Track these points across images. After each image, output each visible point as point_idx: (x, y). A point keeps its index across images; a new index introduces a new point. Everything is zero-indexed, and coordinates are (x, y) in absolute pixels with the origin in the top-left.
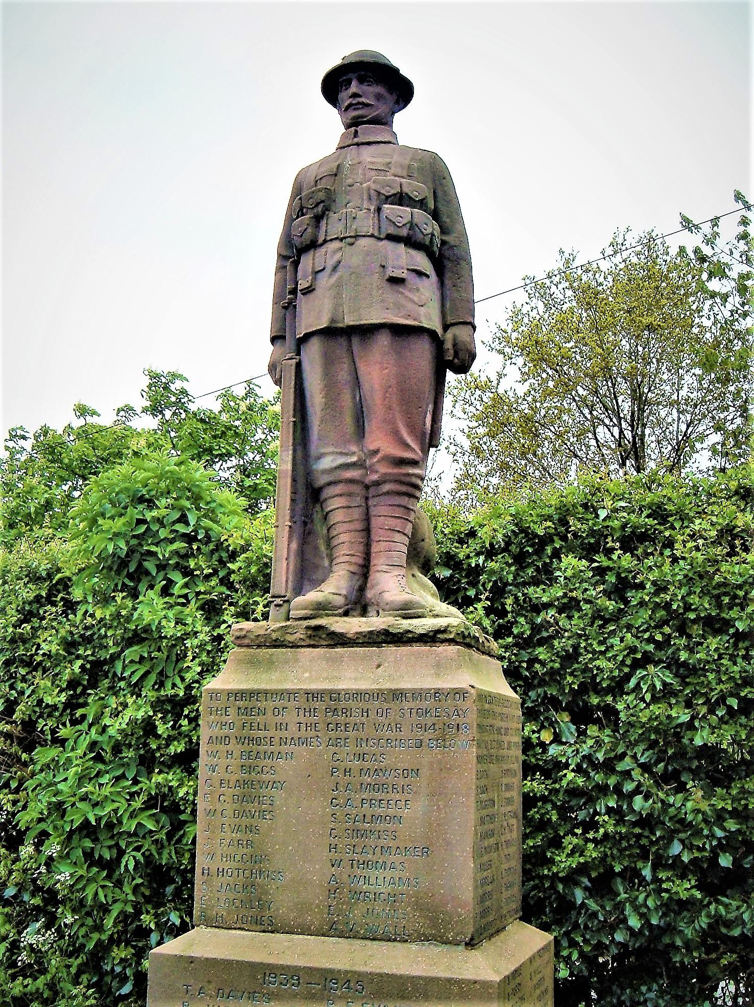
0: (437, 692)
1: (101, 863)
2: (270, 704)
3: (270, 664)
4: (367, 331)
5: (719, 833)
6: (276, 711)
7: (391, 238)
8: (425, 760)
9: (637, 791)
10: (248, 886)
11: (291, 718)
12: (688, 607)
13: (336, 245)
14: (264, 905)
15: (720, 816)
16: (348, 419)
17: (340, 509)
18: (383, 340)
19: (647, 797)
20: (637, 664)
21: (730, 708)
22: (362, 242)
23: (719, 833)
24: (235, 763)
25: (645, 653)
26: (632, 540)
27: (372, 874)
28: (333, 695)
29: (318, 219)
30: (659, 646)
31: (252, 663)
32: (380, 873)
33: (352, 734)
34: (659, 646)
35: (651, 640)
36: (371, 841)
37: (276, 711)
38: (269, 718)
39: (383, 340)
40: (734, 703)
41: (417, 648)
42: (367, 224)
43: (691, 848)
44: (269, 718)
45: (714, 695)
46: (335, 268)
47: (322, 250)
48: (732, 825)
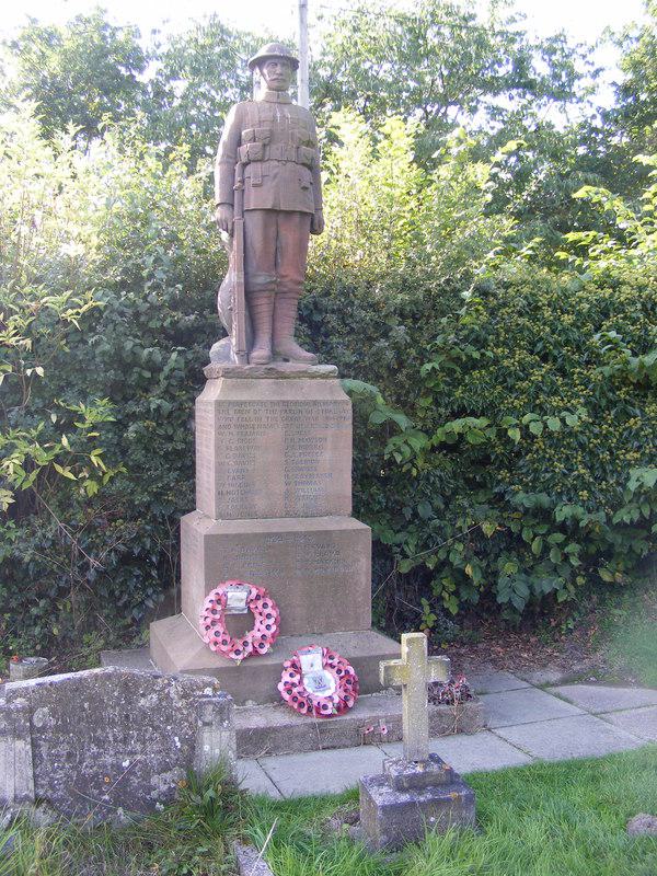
7: (303, 164)
13: (276, 163)
18: (297, 219)
22: (289, 165)
39: (297, 219)
46: (275, 177)
47: (267, 164)
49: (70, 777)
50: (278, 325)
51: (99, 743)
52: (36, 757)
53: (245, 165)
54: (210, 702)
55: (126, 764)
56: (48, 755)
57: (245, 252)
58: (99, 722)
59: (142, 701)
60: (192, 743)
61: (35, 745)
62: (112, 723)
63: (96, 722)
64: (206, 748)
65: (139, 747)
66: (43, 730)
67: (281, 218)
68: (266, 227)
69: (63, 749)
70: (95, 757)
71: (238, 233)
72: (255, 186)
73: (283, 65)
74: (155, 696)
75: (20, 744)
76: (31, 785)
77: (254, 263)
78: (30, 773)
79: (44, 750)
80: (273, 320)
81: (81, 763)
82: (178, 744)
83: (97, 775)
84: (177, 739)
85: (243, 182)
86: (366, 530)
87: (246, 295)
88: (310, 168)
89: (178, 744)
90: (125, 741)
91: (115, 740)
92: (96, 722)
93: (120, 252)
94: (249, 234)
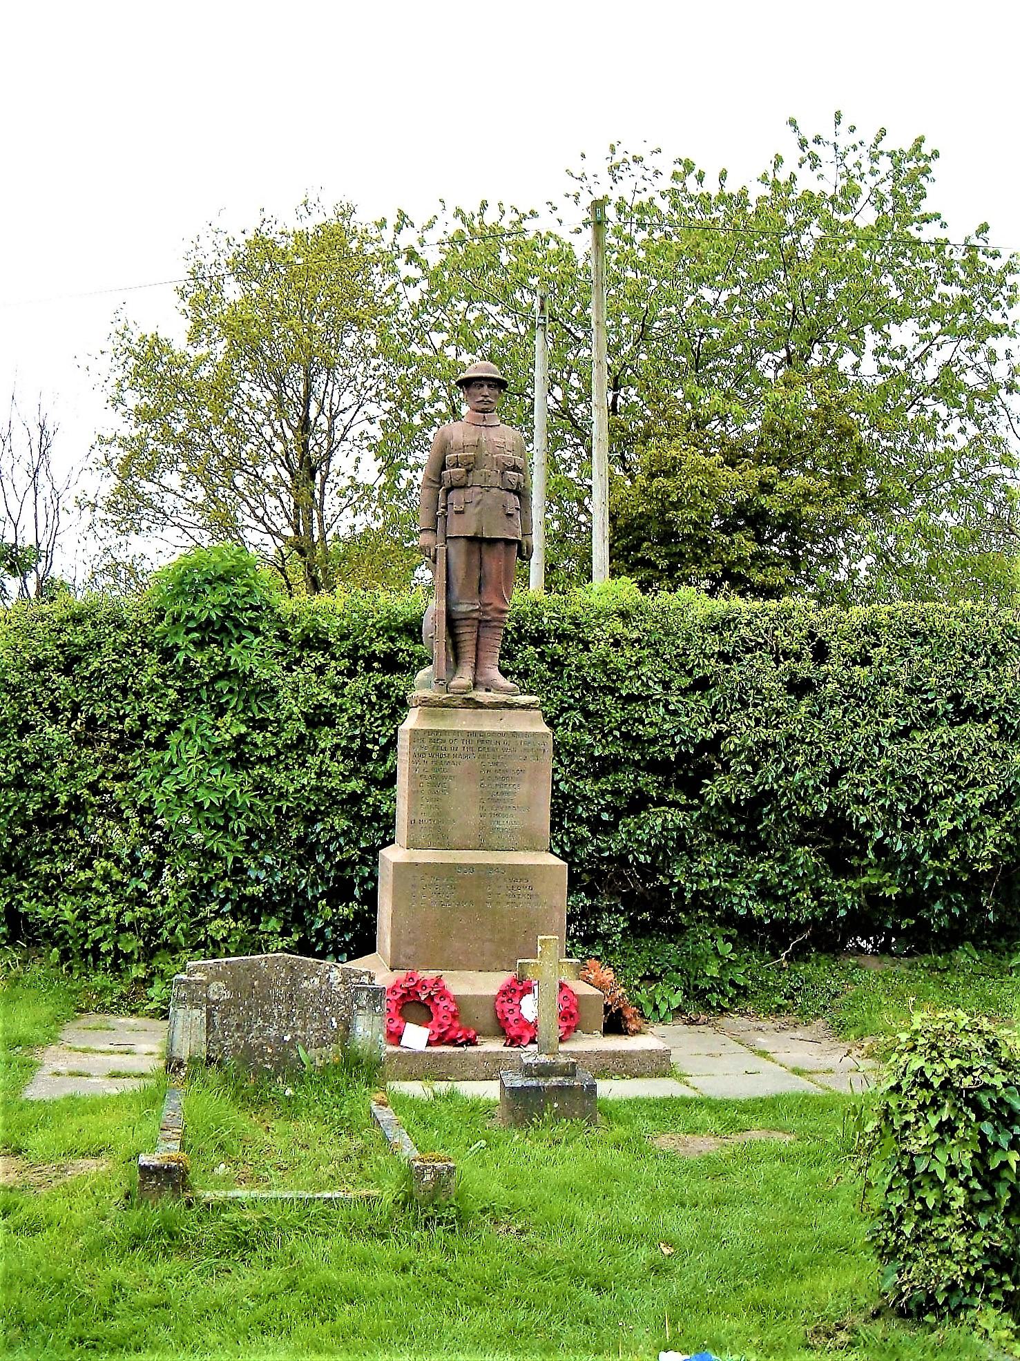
0: (534, 734)
1: (217, 827)
2: (448, 738)
3: (443, 716)
4: (492, 542)
5: (603, 802)
6: (451, 741)
7: (508, 490)
8: (528, 766)
9: (561, 780)
10: (437, 827)
11: (459, 745)
12: (594, 680)
13: (478, 489)
14: (445, 837)
15: (603, 793)
16: (476, 587)
17: (467, 635)
18: (501, 546)
19: (567, 782)
20: (564, 710)
21: (615, 737)
22: (494, 490)
23: (603, 802)
24: (429, 766)
25: (570, 705)
26: (562, 637)
27: (501, 819)
28: (481, 733)
29: (468, 471)
30: (576, 700)
31: (433, 716)
32: (505, 819)
33: (491, 753)
34: (576, 700)
35: (572, 696)
36: (502, 804)
37: (451, 741)
38: (448, 744)
39: (501, 546)
40: (617, 733)
41: (519, 711)
42: (497, 481)
43: (587, 810)
44: (448, 744)
45: (606, 730)
46: (478, 503)
47: (470, 490)
48: (609, 797)
49: (238, 1047)
50: (482, 654)
51: (266, 1017)
52: (210, 1026)
53: (448, 491)
54: (364, 989)
55: (287, 1038)
56: (221, 1024)
57: (448, 579)
58: (266, 998)
59: (306, 983)
60: (347, 1026)
61: (210, 1015)
62: (279, 1001)
63: (263, 998)
64: (360, 1029)
65: (299, 1023)
66: (217, 1002)
67: (484, 546)
68: (469, 553)
69: (233, 1020)
70: (262, 1029)
71: (441, 560)
72: (457, 512)
73: (489, 386)
74: (317, 980)
75: (196, 1012)
76: (204, 1049)
77: (456, 590)
78: (204, 1039)
79: (217, 1020)
80: (477, 649)
81: (248, 1033)
82: (335, 1024)
83: (262, 1045)
84: (334, 1019)
85: (445, 507)
86: (546, 734)
87: (447, 624)
88: (516, 493)
89: (335, 1024)
90: (289, 1017)
91: (280, 1016)
92: (263, 998)
93: (966, 1301)
94: (452, 568)
